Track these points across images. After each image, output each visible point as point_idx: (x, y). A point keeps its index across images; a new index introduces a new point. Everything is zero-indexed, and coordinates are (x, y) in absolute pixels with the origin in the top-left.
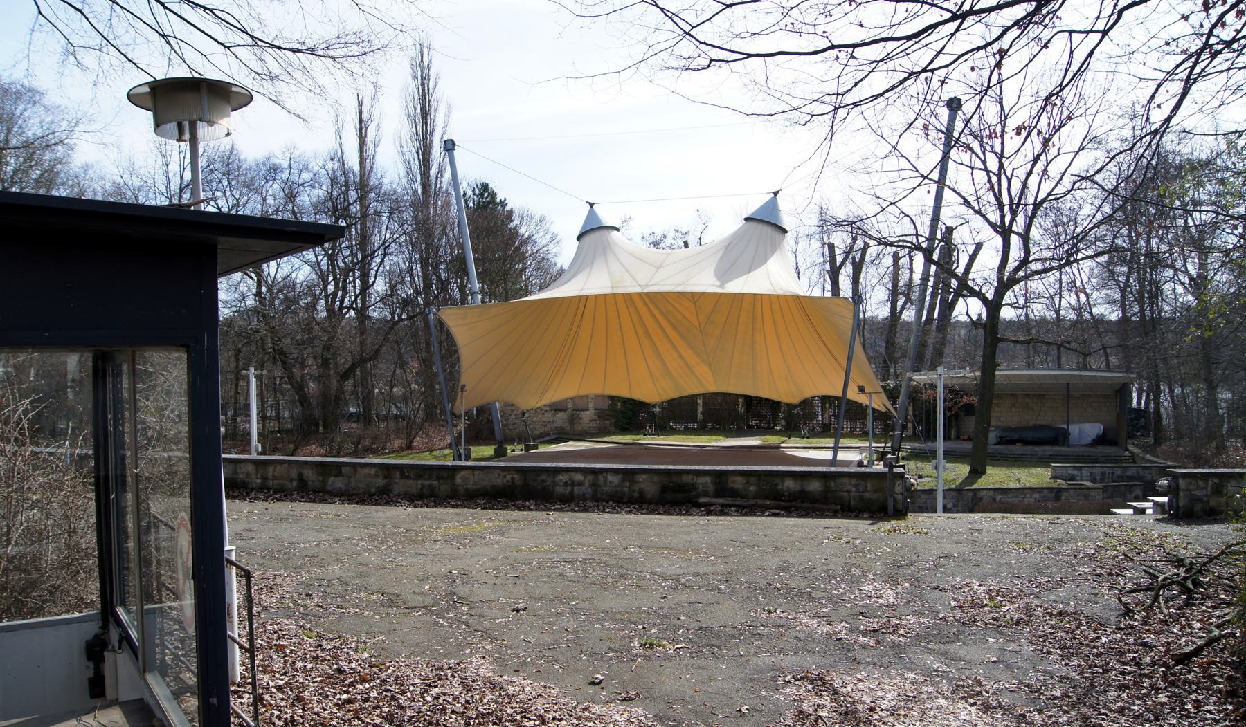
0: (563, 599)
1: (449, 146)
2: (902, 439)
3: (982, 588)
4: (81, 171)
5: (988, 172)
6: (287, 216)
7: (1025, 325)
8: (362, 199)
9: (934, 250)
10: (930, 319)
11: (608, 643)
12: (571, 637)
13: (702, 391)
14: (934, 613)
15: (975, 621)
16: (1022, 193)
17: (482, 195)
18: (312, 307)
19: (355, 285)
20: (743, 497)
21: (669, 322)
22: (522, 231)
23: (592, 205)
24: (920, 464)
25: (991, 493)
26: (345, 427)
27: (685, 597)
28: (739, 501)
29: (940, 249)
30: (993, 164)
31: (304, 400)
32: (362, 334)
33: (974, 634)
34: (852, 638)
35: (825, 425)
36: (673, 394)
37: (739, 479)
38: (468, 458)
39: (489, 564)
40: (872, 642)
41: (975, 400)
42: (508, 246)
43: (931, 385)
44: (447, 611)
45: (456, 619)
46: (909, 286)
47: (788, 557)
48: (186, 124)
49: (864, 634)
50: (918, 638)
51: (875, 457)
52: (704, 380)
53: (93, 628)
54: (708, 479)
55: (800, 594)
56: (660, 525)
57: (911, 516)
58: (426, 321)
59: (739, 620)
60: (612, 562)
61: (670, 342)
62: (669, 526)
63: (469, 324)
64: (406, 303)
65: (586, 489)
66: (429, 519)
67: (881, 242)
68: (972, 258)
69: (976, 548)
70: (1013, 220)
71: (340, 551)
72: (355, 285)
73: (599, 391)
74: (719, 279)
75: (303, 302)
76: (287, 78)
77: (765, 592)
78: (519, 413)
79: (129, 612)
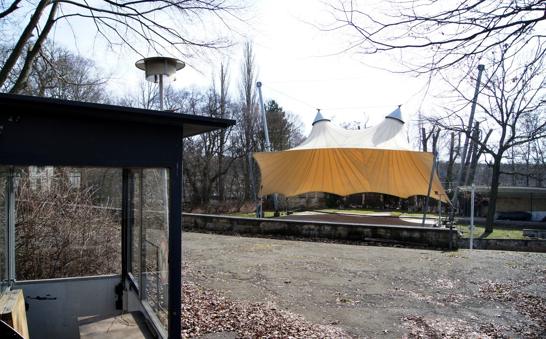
0: (306, 279)
1: (259, 85)
2: (454, 215)
3: (493, 284)
4: (109, 94)
5: (496, 98)
6: (191, 113)
7: (512, 166)
8: (222, 106)
9: (471, 132)
10: (468, 163)
11: (326, 299)
12: (310, 295)
13: (365, 191)
14: (471, 294)
15: (490, 298)
16: (512, 108)
17: (272, 105)
18: (200, 151)
19: (218, 143)
20: (384, 238)
21: (351, 161)
22: (288, 121)
23: (319, 110)
24: (462, 227)
25: (495, 241)
26: (212, 202)
27: (359, 281)
28: (383, 240)
29: (473, 132)
30: (499, 94)
31: (195, 190)
32: (220, 163)
33: (490, 304)
34: (434, 303)
35: (419, 208)
36: (352, 192)
37: (383, 230)
38: (263, 217)
39: (274, 262)
40: (443, 305)
41: (488, 199)
42: (282, 127)
43: (468, 192)
44: (257, 282)
45: (261, 285)
46: (459, 148)
47: (405, 265)
48: (158, 76)
49: (439, 301)
50: (464, 304)
51: (442, 223)
52: (365, 187)
53: (118, 281)
54: (369, 230)
55: (410, 282)
56: (348, 249)
57: (460, 250)
58: (247, 158)
59: (383, 292)
60: (327, 264)
61: (351, 169)
62: (351, 249)
63: (265, 160)
64: (239, 150)
65: (316, 232)
66: (249, 242)
67: (446, 128)
68: (488, 136)
69: (490, 265)
70: (507, 119)
71: (212, 254)
72: (218, 143)
73: (320, 190)
74: (374, 143)
75: (196, 149)
76: (196, 56)
77: (394, 280)
78: (285, 198)
79: (133, 275)
